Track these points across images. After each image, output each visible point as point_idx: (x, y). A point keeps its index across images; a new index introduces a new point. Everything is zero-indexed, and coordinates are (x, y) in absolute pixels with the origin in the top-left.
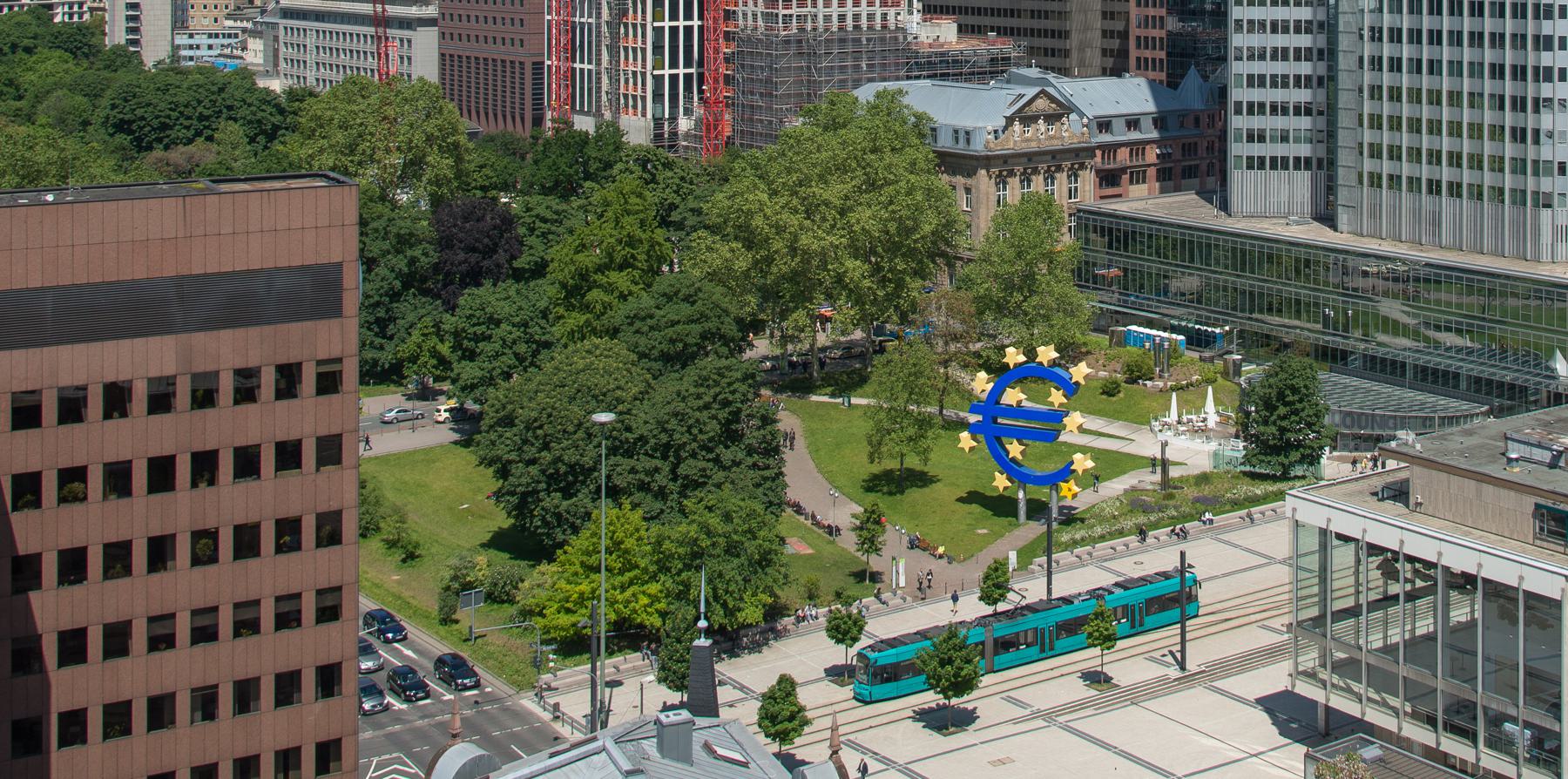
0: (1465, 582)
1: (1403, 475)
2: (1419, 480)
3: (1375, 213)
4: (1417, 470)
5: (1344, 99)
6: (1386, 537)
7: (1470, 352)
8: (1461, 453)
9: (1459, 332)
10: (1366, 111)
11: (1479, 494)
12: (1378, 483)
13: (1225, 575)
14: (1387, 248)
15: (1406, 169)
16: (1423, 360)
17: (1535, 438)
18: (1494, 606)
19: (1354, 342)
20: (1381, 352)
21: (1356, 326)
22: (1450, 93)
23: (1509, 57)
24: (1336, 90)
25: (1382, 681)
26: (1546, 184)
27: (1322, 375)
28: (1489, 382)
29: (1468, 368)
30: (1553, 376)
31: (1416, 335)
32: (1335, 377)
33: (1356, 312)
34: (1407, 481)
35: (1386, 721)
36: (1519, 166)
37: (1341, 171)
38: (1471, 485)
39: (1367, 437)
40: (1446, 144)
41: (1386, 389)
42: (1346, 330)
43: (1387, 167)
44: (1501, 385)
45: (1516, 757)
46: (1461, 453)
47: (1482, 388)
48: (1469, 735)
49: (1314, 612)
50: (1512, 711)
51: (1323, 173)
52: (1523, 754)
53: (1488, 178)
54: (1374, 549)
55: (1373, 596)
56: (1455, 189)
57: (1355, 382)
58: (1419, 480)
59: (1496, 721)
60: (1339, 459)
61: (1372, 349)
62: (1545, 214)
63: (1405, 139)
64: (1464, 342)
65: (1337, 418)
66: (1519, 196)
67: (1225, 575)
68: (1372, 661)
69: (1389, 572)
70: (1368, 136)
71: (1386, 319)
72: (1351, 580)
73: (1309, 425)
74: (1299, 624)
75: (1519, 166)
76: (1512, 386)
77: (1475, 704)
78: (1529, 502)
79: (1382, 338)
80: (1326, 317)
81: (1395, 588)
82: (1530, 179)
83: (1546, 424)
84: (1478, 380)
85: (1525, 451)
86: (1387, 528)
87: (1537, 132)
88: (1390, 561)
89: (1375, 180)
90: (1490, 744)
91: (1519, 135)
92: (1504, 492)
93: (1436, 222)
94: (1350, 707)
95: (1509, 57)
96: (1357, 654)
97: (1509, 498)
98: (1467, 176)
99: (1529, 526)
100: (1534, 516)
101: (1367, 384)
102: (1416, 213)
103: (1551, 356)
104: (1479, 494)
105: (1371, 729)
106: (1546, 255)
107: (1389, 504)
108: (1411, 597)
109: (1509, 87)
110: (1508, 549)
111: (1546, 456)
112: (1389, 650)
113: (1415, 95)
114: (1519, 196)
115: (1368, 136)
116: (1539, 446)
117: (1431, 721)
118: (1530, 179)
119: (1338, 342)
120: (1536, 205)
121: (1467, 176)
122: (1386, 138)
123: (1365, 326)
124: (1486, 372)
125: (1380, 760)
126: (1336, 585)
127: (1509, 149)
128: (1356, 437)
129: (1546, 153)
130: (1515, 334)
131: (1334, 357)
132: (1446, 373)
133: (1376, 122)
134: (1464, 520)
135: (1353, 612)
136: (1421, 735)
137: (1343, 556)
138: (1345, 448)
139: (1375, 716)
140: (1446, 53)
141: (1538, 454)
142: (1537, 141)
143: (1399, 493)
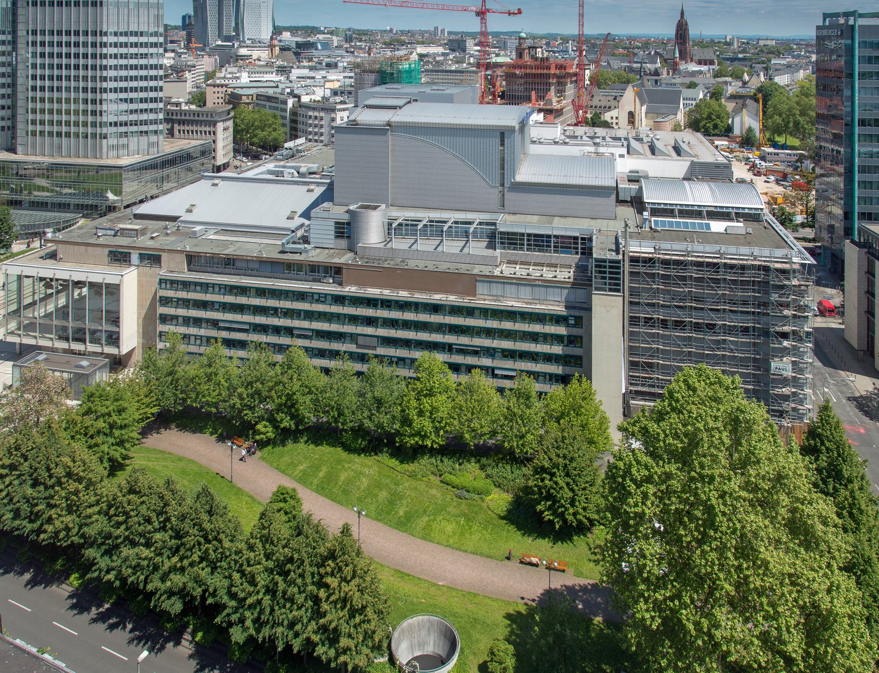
0: (79, 284)
1: (54, 248)
2: (62, 250)
3: (34, 146)
4: (60, 246)
5: (20, 103)
6: (49, 274)
7: (75, 194)
8: (79, 237)
9: (70, 188)
10: (30, 107)
11: (86, 251)
12: (43, 253)
13: (503, 168)
14: (39, 159)
15: (47, 128)
16: (55, 200)
17: (108, 226)
18: (93, 290)
19: (24, 197)
20: (36, 199)
21: (26, 190)
22: (66, 99)
23: (90, 85)
24: (16, 100)
25: (45, 329)
26: (104, 130)
27: (12, 211)
28: (82, 205)
29: (73, 201)
30: (107, 199)
31: (52, 191)
32: (16, 211)
33: (25, 185)
34: (56, 250)
35: (49, 344)
36: (94, 124)
37: (18, 131)
38: (83, 248)
39: (33, 233)
40: (64, 118)
41: (44, 213)
42: (21, 192)
43: (39, 128)
44: (87, 205)
45: (102, 345)
46: (79, 237)
47: (79, 208)
48: (82, 340)
49: (14, 307)
50: (100, 328)
51: (10, 132)
52: (104, 342)
53: (81, 129)
54: (42, 279)
55: (42, 296)
56: (68, 135)
57: (25, 212)
58: (62, 250)
59: (93, 332)
60: (19, 244)
61: (32, 198)
62: (104, 141)
63: (47, 117)
64: (72, 191)
65: (18, 228)
66: (94, 136)
67: (503, 168)
68: (41, 322)
69: (48, 285)
70: (30, 116)
71: (39, 186)
72: (31, 289)
73: (6, 233)
74: (8, 314)
75: (94, 124)
76: (92, 206)
77: (85, 329)
78: (107, 251)
79: (36, 193)
80: (12, 188)
81: (49, 291)
82: (98, 129)
83: (111, 220)
84: (78, 205)
85: (104, 232)
86: (49, 270)
87: (101, 112)
88: (48, 282)
89: (34, 133)
90: (91, 342)
91: (94, 113)
92: (96, 249)
93: (60, 147)
94: (32, 342)
95: (90, 85)
96: (34, 321)
97: (98, 250)
98: (73, 129)
99: (106, 259)
100: (108, 256)
101: (31, 212)
102: (52, 145)
103: (106, 191)
104: (86, 251)
105: (40, 348)
106: (105, 156)
107: (48, 261)
108: (58, 292)
109: (90, 96)
110: (99, 269)
111: (113, 233)
112: (48, 316)
113: (51, 100)
114: (94, 136)
115: (30, 116)
116: (110, 229)
117: (67, 339)
118: (98, 129)
119: (19, 198)
120: (101, 138)
121: (73, 129)
122: (39, 117)
123: (30, 190)
124: (81, 202)
125: (46, 359)
126: (25, 292)
127: (90, 119)
128: (26, 234)
129: (105, 119)
130: (92, 186)
131: (16, 204)
132: (64, 204)
133: (34, 111)
134: (80, 260)
135: (34, 303)
136: (61, 345)
137: (27, 282)
138: (22, 239)
139: (42, 343)
140: (64, 84)
141: (109, 232)
142: (101, 115)
143: (53, 256)
